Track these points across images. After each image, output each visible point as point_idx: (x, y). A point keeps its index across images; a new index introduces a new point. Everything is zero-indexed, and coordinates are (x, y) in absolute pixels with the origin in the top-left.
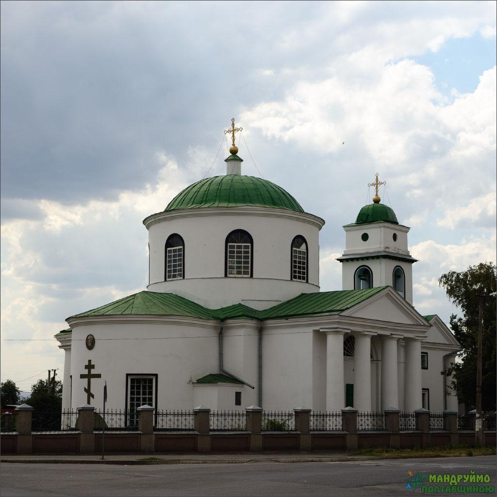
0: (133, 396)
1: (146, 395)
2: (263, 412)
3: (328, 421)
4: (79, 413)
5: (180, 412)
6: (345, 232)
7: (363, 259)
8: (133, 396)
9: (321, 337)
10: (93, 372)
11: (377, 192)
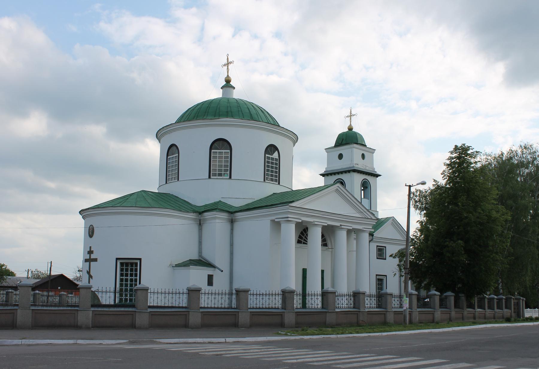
0: (122, 277)
2: (366, 294)
3: (310, 299)
4: (188, 293)
5: (271, 292)
7: (338, 173)
8: (122, 277)
9: (276, 225)
10: (93, 256)
11: (351, 122)
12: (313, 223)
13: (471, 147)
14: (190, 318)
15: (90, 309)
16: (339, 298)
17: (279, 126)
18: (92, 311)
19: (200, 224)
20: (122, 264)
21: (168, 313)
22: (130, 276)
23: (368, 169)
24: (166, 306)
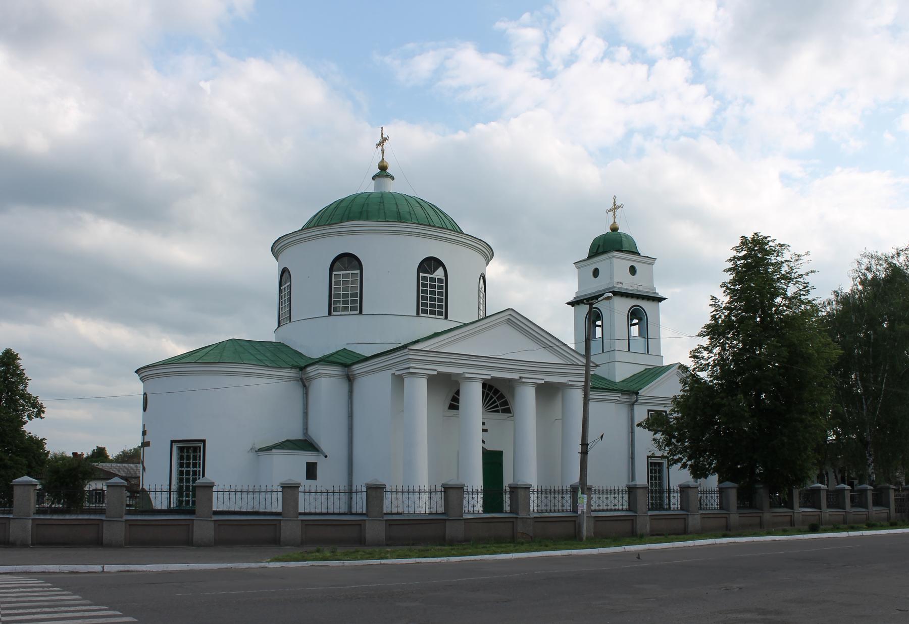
1: (186, 471)
6: (577, 270)
11: (615, 218)
12: (463, 376)
13: (770, 237)
14: (194, 530)
15: (211, 518)
16: (708, 495)
17: (462, 232)
18: (32, 519)
19: (304, 386)
20: (181, 449)
21: (157, 523)
22: (193, 467)
23: (643, 289)
24: (307, 512)
